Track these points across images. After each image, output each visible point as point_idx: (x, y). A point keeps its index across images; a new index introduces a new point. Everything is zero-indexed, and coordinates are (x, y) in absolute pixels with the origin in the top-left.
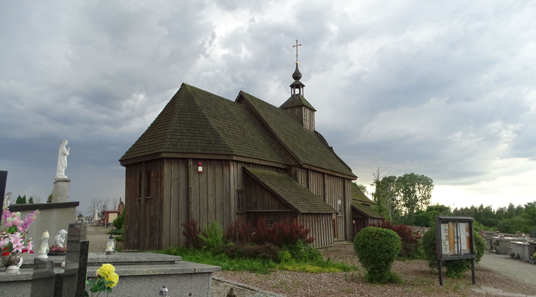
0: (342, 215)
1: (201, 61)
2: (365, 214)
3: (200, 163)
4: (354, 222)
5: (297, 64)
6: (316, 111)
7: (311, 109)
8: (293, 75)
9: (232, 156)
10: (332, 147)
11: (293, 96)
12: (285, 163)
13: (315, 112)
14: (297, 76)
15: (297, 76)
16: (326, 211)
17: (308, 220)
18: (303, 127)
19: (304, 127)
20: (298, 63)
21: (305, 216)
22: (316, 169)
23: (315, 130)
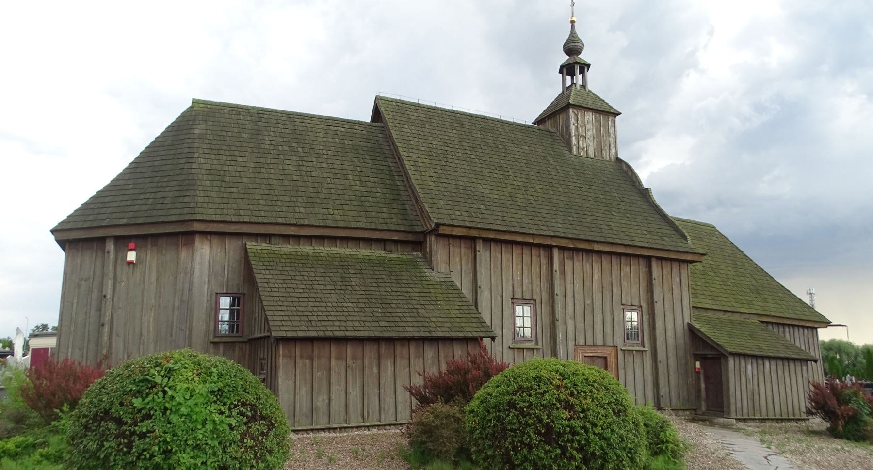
0: (644, 347)
1: (691, 83)
2: (718, 345)
3: (132, 245)
4: (698, 365)
5: (573, 22)
6: (619, 114)
7: (599, 110)
8: (564, 45)
9: (190, 223)
10: (648, 190)
11: (567, 90)
12: (408, 229)
13: (617, 117)
14: (572, 48)
15: (572, 48)
16: (430, 332)
17: (793, 372)
18: (570, 150)
19: (575, 152)
20: (574, 19)
21: (780, 363)
22: (531, 241)
23: (620, 156)
